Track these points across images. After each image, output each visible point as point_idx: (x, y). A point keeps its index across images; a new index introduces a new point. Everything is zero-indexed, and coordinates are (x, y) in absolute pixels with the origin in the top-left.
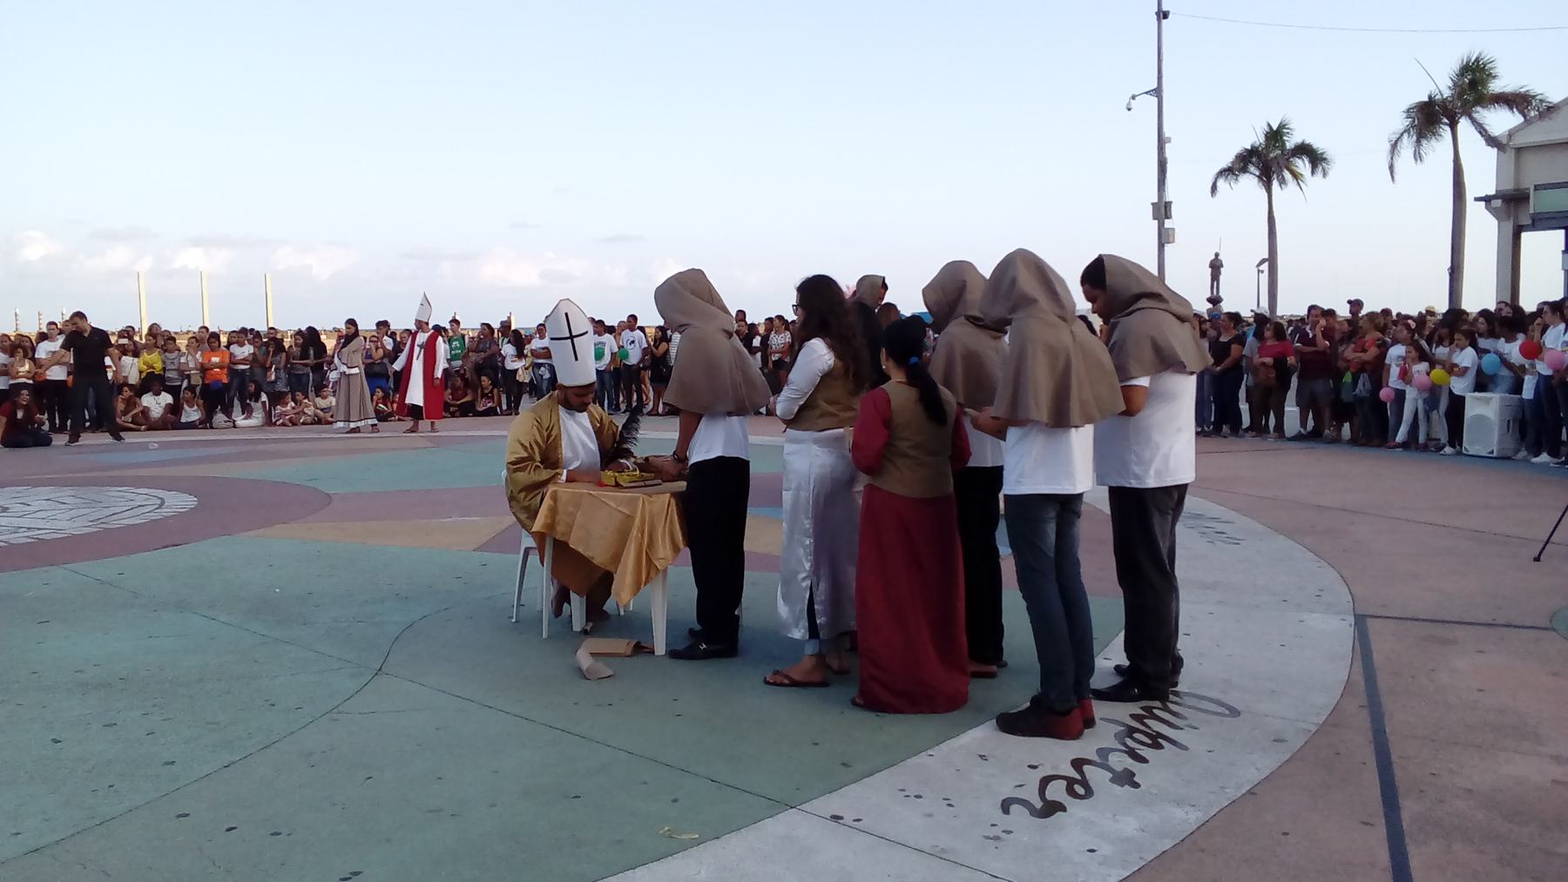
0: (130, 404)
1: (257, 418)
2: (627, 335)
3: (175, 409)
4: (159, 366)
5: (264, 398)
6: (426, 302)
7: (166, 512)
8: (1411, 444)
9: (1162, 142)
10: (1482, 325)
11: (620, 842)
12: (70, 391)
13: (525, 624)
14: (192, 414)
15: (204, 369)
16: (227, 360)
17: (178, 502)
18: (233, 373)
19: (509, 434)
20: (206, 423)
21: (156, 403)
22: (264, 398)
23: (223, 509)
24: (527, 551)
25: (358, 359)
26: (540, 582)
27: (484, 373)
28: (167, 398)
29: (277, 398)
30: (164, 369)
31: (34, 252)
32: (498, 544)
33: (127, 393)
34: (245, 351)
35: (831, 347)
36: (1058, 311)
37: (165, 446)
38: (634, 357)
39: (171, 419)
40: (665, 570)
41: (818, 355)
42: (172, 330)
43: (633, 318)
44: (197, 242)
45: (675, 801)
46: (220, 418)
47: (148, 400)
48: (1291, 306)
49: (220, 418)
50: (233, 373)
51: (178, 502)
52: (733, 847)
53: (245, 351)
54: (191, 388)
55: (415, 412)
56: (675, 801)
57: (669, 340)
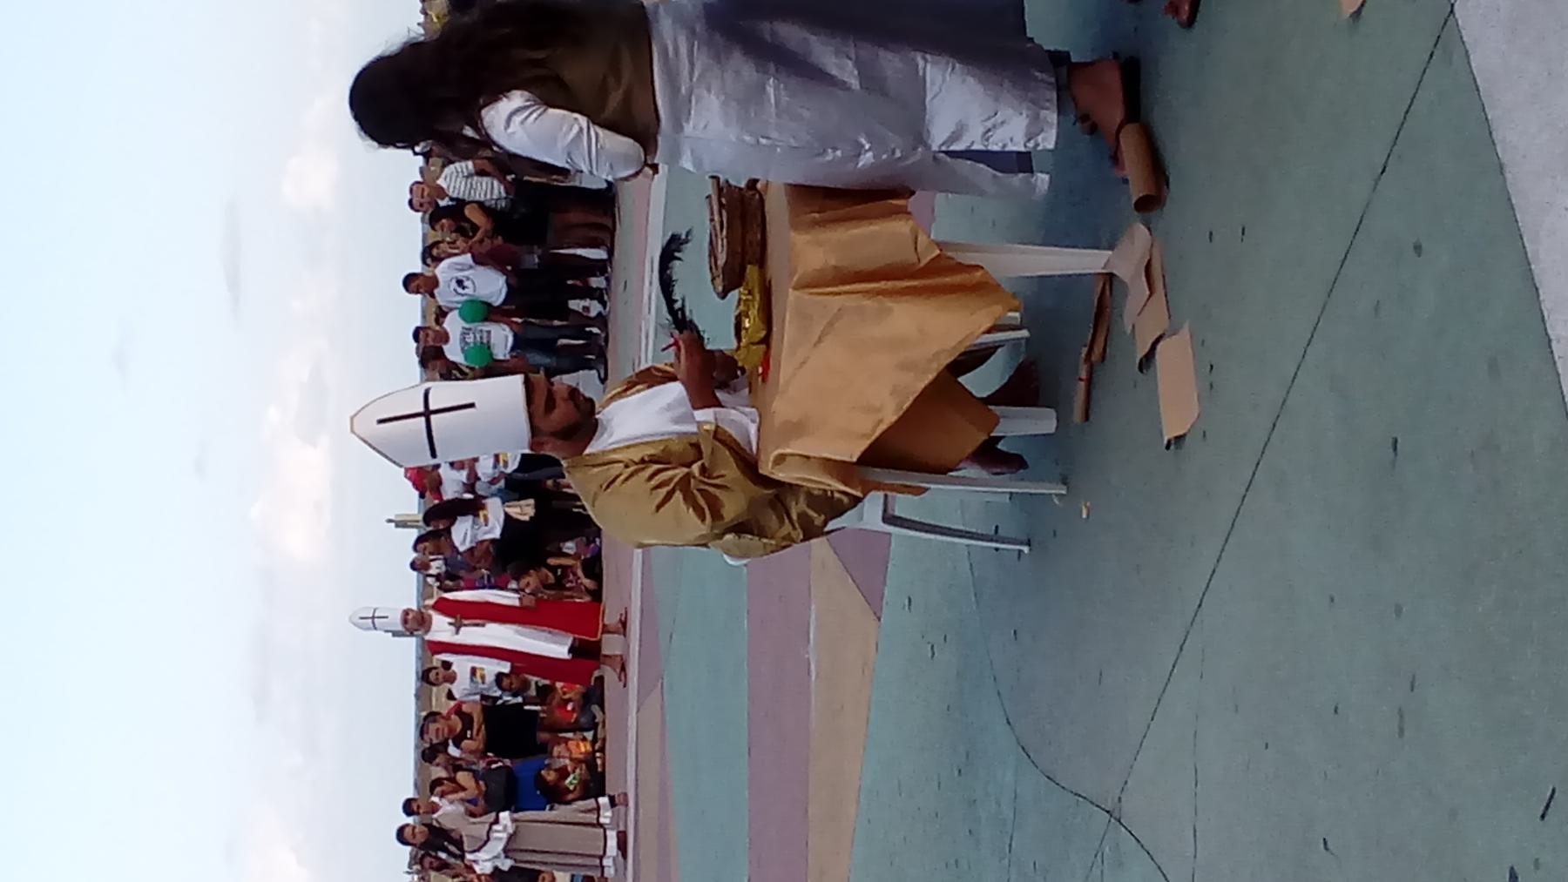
2: (445, 295)
6: (372, 621)
11: (1493, 367)
12: (508, 749)
13: (1034, 532)
19: (656, 564)
24: (889, 519)
25: (477, 828)
26: (962, 497)
27: (518, 539)
32: (868, 570)
35: (495, 96)
36: (611, 81)
38: (492, 285)
40: (939, 245)
41: (514, 122)
43: (411, 282)
45: (1418, 248)
52: (1522, 138)
55: (587, 652)
56: (1418, 248)
57: (460, 203)
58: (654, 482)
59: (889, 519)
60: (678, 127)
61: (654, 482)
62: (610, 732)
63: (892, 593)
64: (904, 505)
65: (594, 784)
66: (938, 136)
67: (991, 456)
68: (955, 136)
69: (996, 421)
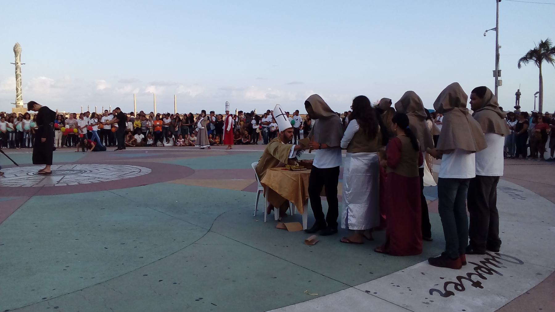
2: (295, 117)
13: (258, 216)
24: (260, 191)
26: (264, 203)
27: (246, 129)
41: (354, 126)
45: (310, 281)
52: (331, 300)
56: (310, 281)
58: (498, 256)
59: (260, 191)
60: (353, 157)
61: (498, 256)
62: (220, 146)
63: (245, 193)
64: (262, 194)
65: (212, 144)
66: (351, 206)
67: (271, 208)
68: (351, 210)
69: (277, 208)
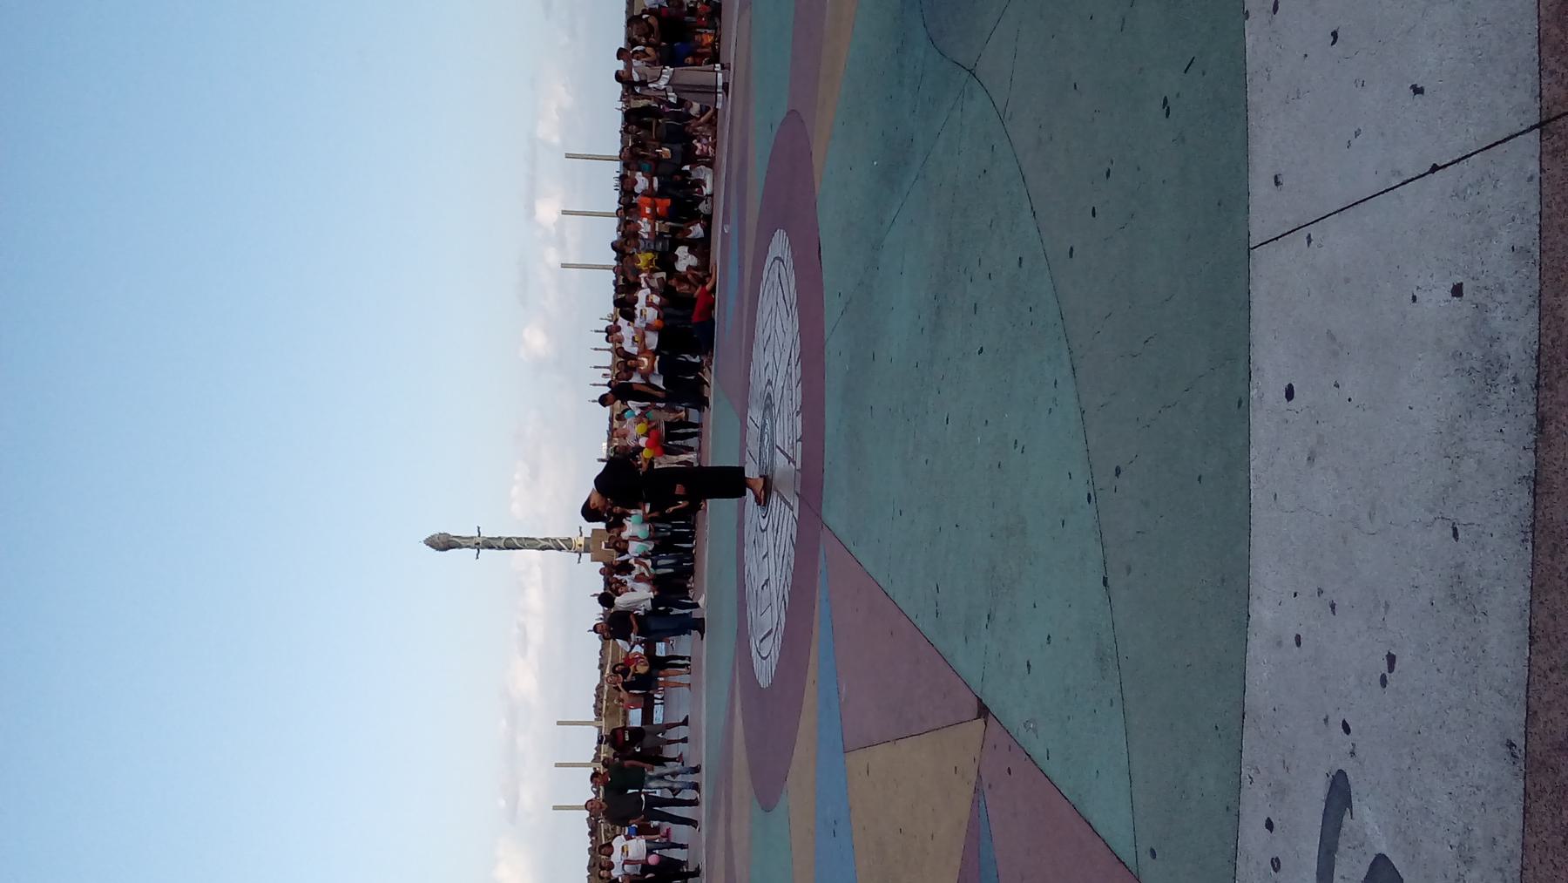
0: (682, 278)
1: (705, 174)
3: (693, 246)
4: (650, 256)
5: (687, 168)
7: (787, 256)
8: (714, 146)
9: (510, 545)
10: (631, 227)
14: (697, 230)
15: (654, 217)
16: (649, 200)
17: (780, 244)
18: (661, 193)
20: (708, 221)
21: (685, 260)
22: (687, 168)
23: (791, 206)
28: (682, 251)
29: (690, 157)
30: (654, 251)
31: (537, 340)
33: (673, 282)
34: (642, 183)
37: (726, 221)
39: (701, 248)
42: (603, 450)
44: (531, 211)
46: (703, 207)
47: (681, 266)
48: (615, 263)
49: (703, 207)
50: (661, 193)
51: (780, 244)
53: (642, 183)
54: (673, 230)
